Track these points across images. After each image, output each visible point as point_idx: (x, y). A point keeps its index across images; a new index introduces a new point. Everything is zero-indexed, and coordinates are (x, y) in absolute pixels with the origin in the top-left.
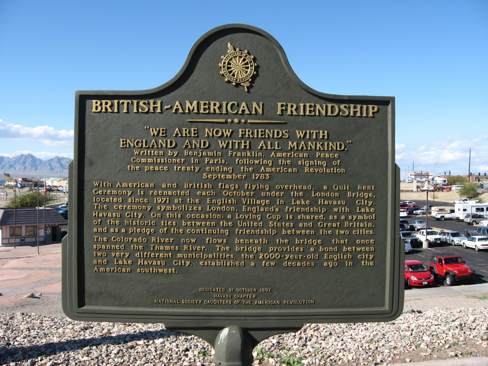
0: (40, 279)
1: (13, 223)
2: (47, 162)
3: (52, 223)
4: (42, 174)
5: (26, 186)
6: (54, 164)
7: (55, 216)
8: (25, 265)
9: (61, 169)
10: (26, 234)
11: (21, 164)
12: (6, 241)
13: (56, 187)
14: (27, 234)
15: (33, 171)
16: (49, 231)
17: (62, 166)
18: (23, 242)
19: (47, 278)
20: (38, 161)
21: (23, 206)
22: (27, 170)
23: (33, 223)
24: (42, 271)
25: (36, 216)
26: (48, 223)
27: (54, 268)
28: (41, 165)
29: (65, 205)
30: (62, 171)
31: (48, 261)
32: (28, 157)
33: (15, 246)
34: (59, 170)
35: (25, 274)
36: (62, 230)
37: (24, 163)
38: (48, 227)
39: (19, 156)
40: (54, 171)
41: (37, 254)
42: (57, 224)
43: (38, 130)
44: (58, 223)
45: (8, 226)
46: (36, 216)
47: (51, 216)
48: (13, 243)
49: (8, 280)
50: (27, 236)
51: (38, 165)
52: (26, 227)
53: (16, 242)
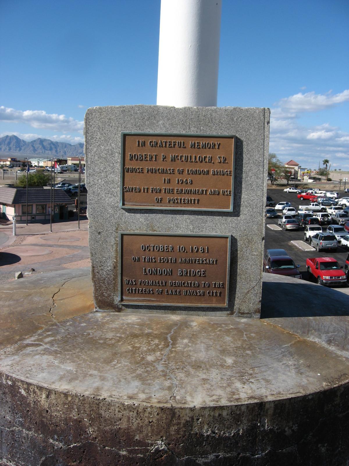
0: (62, 256)
1: (25, 201)
2: (30, 143)
3: (60, 203)
4: (26, 154)
5: (14, 165)
6: (37, 146)
7: (62, 196)
8: (44, 242)
9: (43, 150)
10: (36, 212)
11: (6, 145)
12: (19, 218)
13: (43, 167)
14: (38, 212)
15: (17, 151)
16: (57, 211)
17: (44, 147)
18: (34, 219)
19: (69, 255)
20: (22, 142)
21: (31, 185)
22: (11, 151)
23: (43, 202)
24: (60, 249)
25: (49, 196)
26: (57, 203)
27: (72, 246)
28: (25, 146)
29: (60, 185)
30: (44, 152)
31: (63, 239)
32: (13, 139)
33: (27, 223)
34: (41, 151)
35: (47, 251)
36: (69, 209)
37: (9, 143)
38: (56, 206)
40: (36, 152)
41: (50, 232)
42: (64, 203)
43: (27, 113)
44: (65, 203)
45: (21, 205)
46: (49, 196)
47: (60, 196)
48: (25, 221)
49: (34, 256)
50: (37, 214)
51: (22, 146)
52: (37, 205)
53: (28, 219)
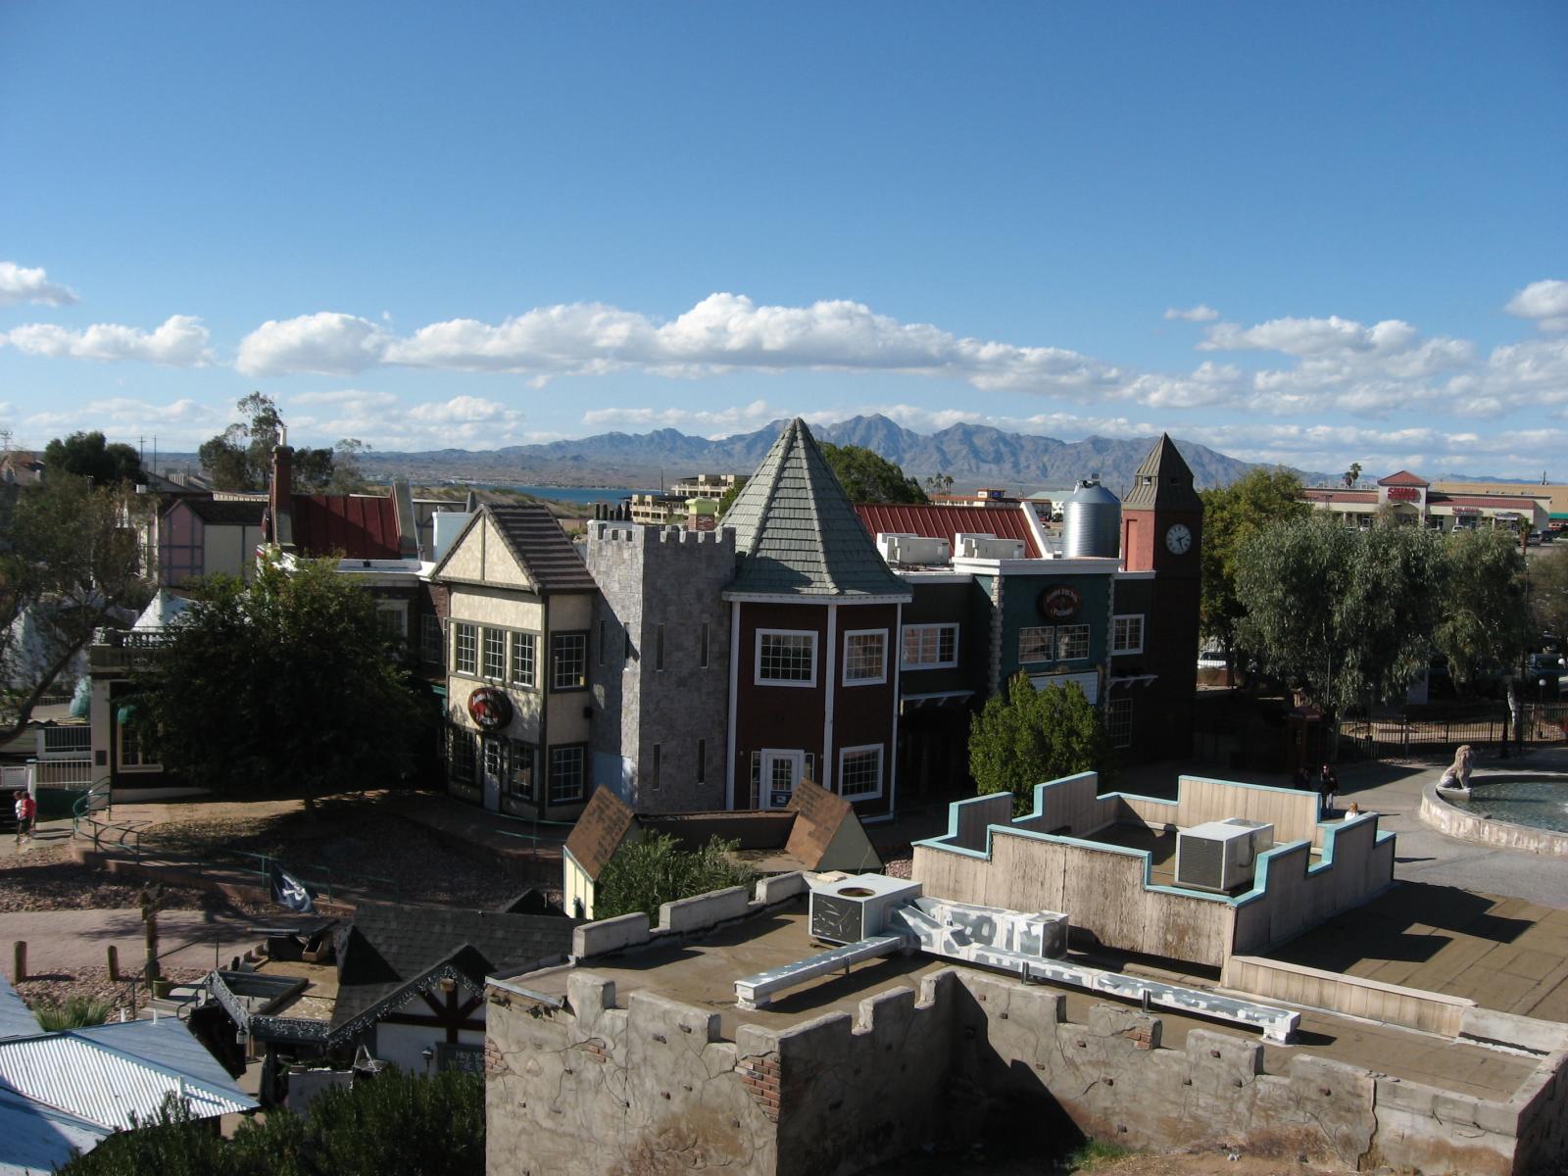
6: (952, 447)
9: (973, 462)
17: (976, 453)
20: (905, 438)
28: (914, 450)
30: (975, 470)
34: (966, 467)
39: (850, 421)
51: (904, 451)
